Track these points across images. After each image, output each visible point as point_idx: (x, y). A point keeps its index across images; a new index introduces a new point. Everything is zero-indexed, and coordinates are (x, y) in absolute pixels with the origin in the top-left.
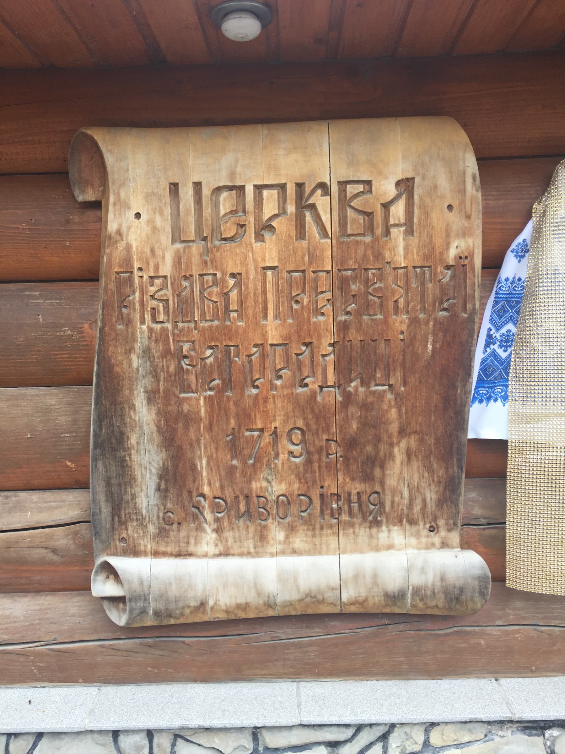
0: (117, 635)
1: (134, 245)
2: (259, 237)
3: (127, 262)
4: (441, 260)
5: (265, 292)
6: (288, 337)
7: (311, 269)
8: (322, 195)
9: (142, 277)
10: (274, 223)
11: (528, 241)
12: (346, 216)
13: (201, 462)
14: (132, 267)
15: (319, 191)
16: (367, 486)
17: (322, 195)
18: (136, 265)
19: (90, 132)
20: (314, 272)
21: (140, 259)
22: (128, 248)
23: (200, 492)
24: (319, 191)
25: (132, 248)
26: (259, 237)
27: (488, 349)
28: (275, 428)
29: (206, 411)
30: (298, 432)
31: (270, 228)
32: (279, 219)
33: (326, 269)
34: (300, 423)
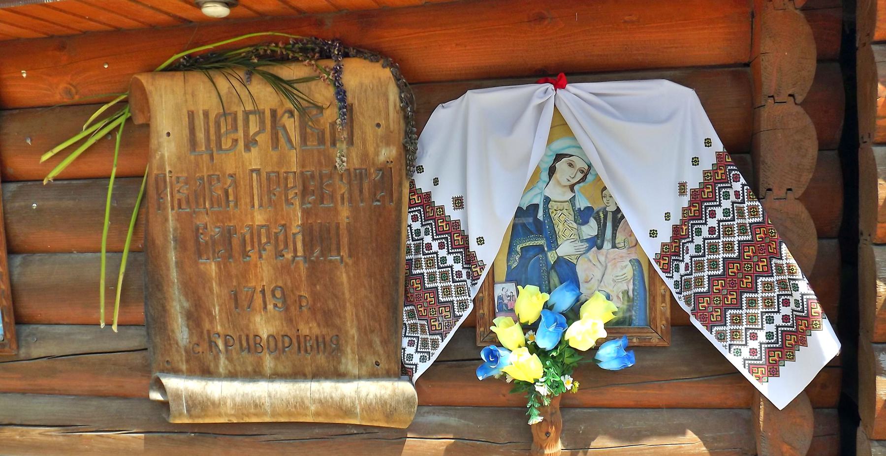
0: (168, 429)
1: (166, 155)
2: (247, 148)
3: (162, 167)
4: (373, 164)
5: (252, 187)
6: (268, 220)
7: (283, 171)
8: (289, 117)
9: (171, 177)
10: (257, 138)
11: (230, 368)
12: (306, 133)
13: (215, 309)
14: (165, 170)
15: (287, 115)
16: (329, 330)
17: (289, 117)
18: (168, 169)
19: (139, 77)
20: (285, 173)
21: (170, 165)
22: (162, 157)
23: (215, 330)
24: (287, 115)
25: (165, 157)
26: (247, 148)
27: (300, 59)
28: (264, 286)
29: (216, 273)
30: (279, 289)
31: (256, 142)
32: (260, 135)
33: (293, 171)
34: (280, 284)
